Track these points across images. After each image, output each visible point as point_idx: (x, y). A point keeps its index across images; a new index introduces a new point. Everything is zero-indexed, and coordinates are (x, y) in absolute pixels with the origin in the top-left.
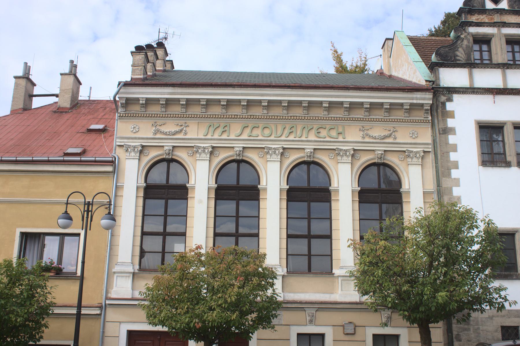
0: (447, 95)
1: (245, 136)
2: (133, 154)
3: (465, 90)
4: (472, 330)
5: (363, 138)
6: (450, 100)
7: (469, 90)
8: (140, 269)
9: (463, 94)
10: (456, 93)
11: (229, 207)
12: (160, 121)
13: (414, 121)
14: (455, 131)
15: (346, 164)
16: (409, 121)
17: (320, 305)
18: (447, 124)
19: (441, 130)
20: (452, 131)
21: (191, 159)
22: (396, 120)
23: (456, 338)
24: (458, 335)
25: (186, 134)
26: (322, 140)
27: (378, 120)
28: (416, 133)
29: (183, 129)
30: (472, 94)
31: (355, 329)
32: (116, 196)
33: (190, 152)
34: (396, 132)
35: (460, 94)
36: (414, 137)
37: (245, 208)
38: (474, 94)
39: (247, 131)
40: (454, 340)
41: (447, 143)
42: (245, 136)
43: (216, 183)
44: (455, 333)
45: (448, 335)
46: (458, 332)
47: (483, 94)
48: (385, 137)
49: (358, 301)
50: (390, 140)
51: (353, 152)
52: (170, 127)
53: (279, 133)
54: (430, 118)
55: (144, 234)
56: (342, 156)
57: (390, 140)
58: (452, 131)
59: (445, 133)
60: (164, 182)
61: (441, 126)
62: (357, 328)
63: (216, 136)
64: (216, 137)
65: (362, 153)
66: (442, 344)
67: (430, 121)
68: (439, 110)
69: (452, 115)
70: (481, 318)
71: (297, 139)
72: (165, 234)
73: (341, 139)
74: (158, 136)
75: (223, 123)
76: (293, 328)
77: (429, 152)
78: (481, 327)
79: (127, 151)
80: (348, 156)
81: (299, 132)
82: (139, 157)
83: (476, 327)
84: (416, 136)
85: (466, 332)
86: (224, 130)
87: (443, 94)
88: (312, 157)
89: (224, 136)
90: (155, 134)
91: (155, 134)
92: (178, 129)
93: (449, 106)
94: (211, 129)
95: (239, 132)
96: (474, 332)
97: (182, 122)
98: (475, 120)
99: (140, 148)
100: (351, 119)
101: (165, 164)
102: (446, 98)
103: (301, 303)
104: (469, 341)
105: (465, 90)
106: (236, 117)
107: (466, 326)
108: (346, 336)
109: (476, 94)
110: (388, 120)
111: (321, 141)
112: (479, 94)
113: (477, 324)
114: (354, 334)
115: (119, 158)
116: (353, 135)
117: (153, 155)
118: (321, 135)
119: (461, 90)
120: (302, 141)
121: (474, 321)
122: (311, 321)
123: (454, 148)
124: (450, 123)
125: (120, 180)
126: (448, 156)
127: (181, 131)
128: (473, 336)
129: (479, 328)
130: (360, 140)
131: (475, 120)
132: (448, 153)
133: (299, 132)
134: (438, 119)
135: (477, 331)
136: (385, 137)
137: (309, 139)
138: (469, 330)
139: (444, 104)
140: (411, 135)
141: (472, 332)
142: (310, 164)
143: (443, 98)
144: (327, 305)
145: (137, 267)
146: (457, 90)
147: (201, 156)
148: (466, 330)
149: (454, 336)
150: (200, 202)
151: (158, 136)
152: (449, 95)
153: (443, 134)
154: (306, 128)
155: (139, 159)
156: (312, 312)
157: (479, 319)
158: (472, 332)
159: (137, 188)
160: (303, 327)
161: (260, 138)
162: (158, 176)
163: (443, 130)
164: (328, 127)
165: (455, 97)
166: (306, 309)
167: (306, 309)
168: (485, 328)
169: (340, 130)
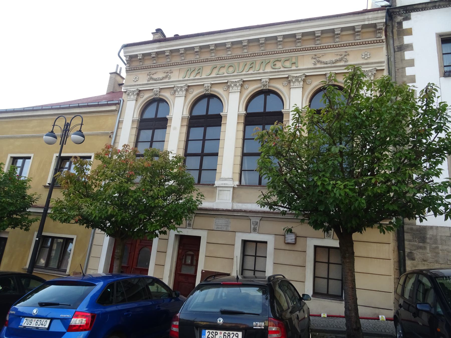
0: (404, 15)
1: (213, 75)
2: (132, 97)
3: (424, 6)
4: (428, 249)
5: (315, 64)
6: (408, 18)
7: (430, 5)
8: (240, 185)
9: (422, 10)
10: (414, 11)
11: (197, 132)
12: (153, 71)
13: (329, 47)
14: (412, 47)
15: (297, 89)
16: (367, 43)
17: (263, 214)
18: (403, 41)
19: (396, 48)
20: (410, 47)
21: (172, 97)
22: (348, 45)
23: (408, 256)
24: (411, 253)
25: (170, 78)
26: (276, 70)
27: (329, 47)
28: (369, 54)
29: (343, 57)
30: (433, 9)
31: (296, 239)
32: (118, 128)
33: (172, 92)
34: (347, 56)
35: (419, 11)
36: (366, 58)
37: (211, 131)
38: (436, 8)
39: (215, 71)
40: (407, 258)
41: (403, 59)
42: (213, 75)
43: (246, 109)
44: (407, 251)
45: (399, 253)
46: (410, 250)
47: (447, 7)
48: (337, 61)
49: (230, 208)
50: (342, 63)
51: (304, 78)
52: (160, 74)
53: (241, 70)
54: (384, 37)
55: (244, 155)
56: (294, 82)
57: (342, 63)
58: (410, 47)
59: (401, 51)
60: (262, 110)
61: (397, 44)
62: (297, 238)
63: (192, 77)
64: (192, 78)
65: (313, 78)
66: (392, 261)
67: (384, 41)
68: (395, 30)
69: (409, 32)
70: (441, 236)
71: (255, 72)
72: (202, 155)
73: (294, 68)
74: (151, 82)
75: (197, 66)
76: (237, 234)
77: (384, 70)
78: (440, 247)
79: (128, 95)
80: (299, 82)
81: (257, 67)
82: (241, 90)
83: (434, 246)
84: (369, 56)
85: (421, 251)
86: (251, 66)
87: (400, 15)
88: (209, 90)
89: (198, 77)
90: (148, 81)
91: (148, 81)
92: (164, 75)
93: (406, 25)
94: (189, 72)
95: (209, 72)
96: (430, 251)
97: (167, 69)
98: (436, 34)
99: (137, 92)
100: (304, 49)
101: (262, 96)
102: (403, 17)
103: (245, 211)
104: (424, 261)
105: (424, 6)
106: (207, 61)
107: (421, 244)
108: (287, 245)
109: (438, 8)
110: (282, 52)
111: (275, 72)
112: (441, 8)
113: (435, 242)
114: (295, 244)
115: (124, 101)
116: (306, 63)
117: (147, 96)
118: (277, 67)
119: (420, 6)
120: (259, 73)
121: (431, 239)
122: (255, 230)
123: (411, 63)
124: (407, 40)
125: (122, 117)
126: (404, 72)
127: (166, 77)
128: (429, 255)
129: (437, 248)
130: (312, 66)
131: (436, 34)
132: (404, 68)
133: (257, 67)
134: (393, 38)
135: (435, 250)
136: (163, 78)
137: (266, 71)
138: (425, 248)
139: (400, 24)
140: (363, 57)
141: (428, 251)
142: (209, 97)
143: (399, 18)
144: (219, 212)
145: (237, 183)
146: (415, 7)
147: (295, 84)
148: (421, 248)
149: (406, 254)
150: (175, 129)
151: (151, 82)
152: (407, 15)
153: (398, 51)
154: (264, 63)
155: (185, 97)
156: (257, 221)
157: (438, 237)
158: (428, 251)
159: (238, 116)
160: (247, 234)
161: (226, 74)
162: (257, 107)
163: (398, 48)
164: (227, 66)
165: (413, 15)
166: (251, 218)
167: (251, 218)
168: (445, 247)
169: (294, 61)
